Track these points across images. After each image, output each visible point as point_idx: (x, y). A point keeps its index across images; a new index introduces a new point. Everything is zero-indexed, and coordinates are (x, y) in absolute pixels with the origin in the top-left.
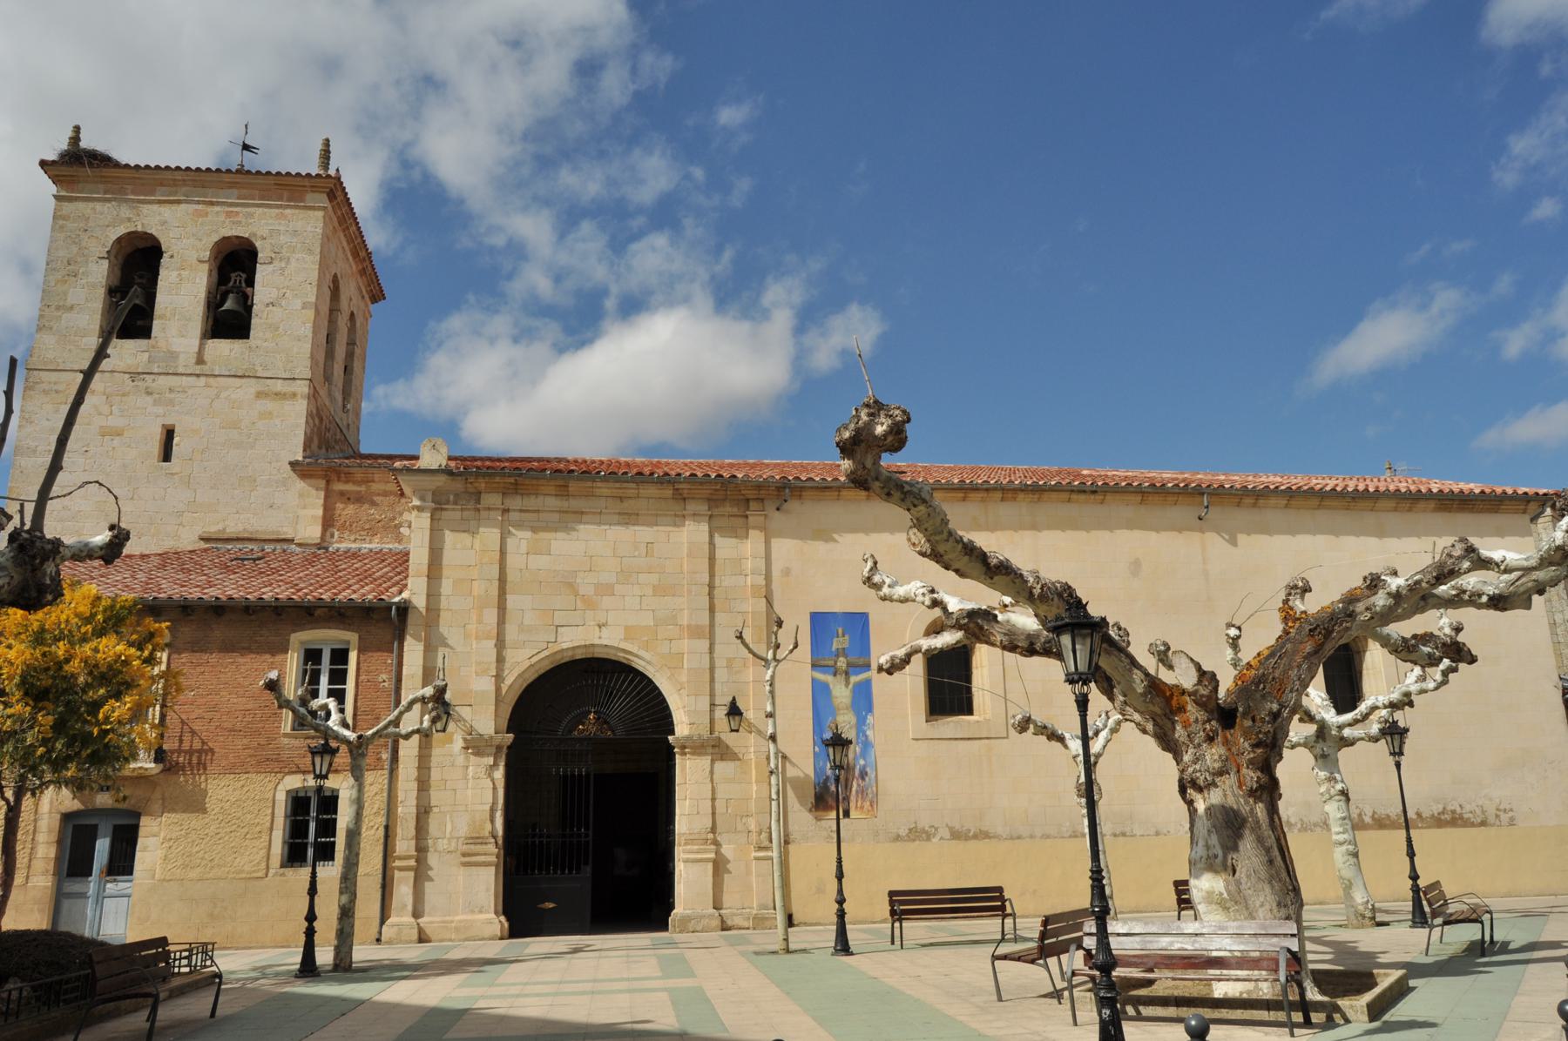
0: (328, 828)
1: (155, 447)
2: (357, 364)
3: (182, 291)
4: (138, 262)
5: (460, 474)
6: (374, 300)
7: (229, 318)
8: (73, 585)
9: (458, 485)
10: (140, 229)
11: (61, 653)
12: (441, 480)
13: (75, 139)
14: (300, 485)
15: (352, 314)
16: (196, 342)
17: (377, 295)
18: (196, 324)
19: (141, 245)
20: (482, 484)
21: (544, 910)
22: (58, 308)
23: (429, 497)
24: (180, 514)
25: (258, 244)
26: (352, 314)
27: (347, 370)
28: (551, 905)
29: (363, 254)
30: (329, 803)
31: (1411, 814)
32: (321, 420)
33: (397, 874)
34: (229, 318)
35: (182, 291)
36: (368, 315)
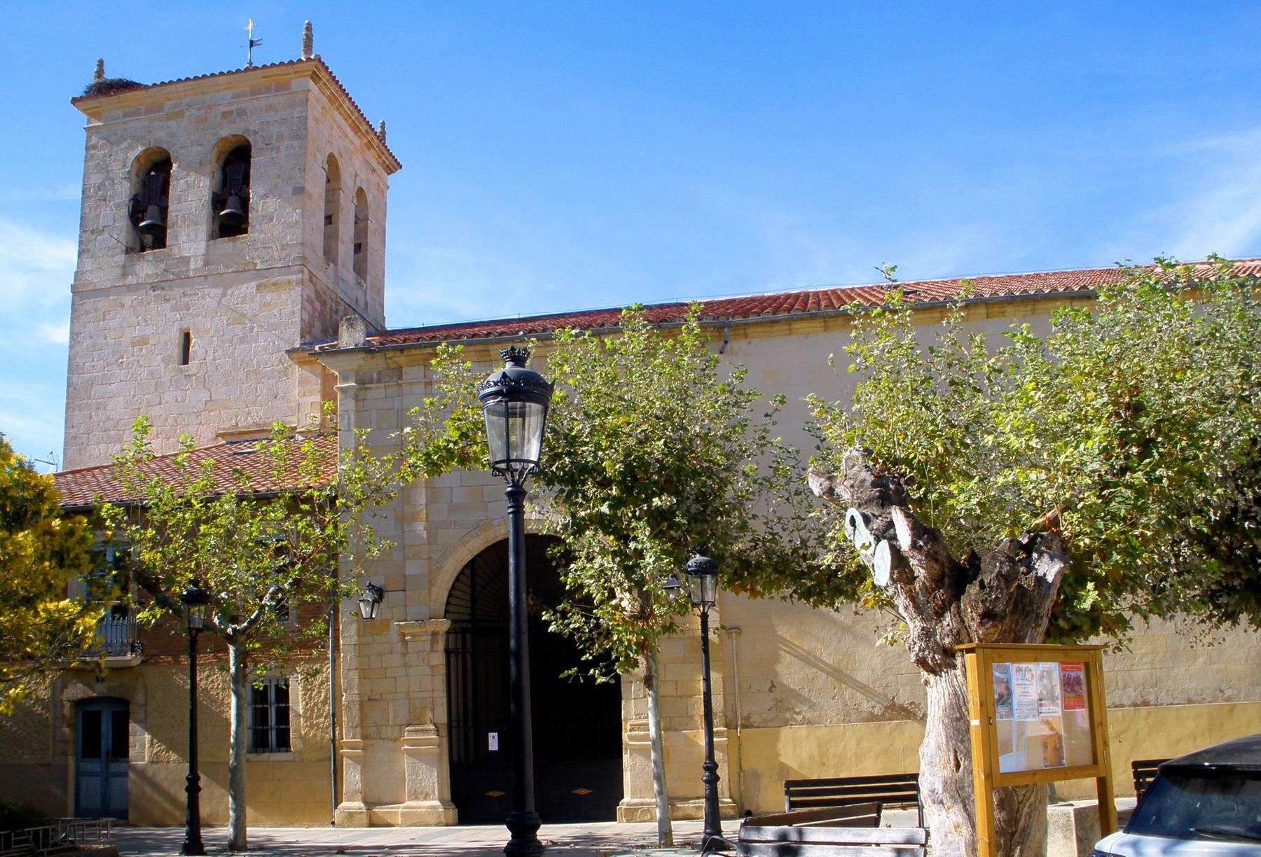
0: (283, 715)
1: (175, 351)
2: (372, 242)
3: (191, 194)
4: (155, 177)
5: (380, 350)
6: (390, 171)
7: (231, 219)
8: (73, 496)
9: (378, 362)
10: (152, 144)
11: (677, 519)
12: (359, 360)
13: (100, 73)
14: (297, 371)
15: (360, 190)
16: (203, 244)
17: (392, 166)
18: (203, 229)
19: (156, 158)
20: (401, 359)
21: (491, 797)
22: (93, 232)
23: (352, 375)
24: (198, 414)
25: (251, 139)
26: (360, 190)
27: (358, 248)
28: (584, 792)
29: (364, 128)
30: (283, 695)
31: (185, 660)
32: (324, 303)
33: (345, 761)
34: (231, 219)
35: (191, 194)
36: (382, 190)
